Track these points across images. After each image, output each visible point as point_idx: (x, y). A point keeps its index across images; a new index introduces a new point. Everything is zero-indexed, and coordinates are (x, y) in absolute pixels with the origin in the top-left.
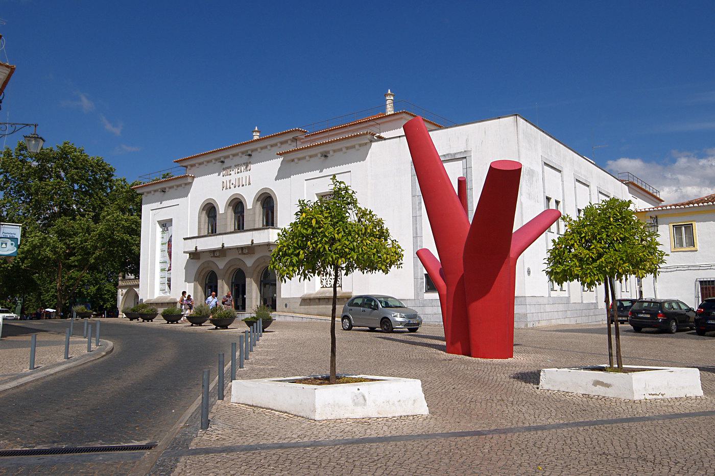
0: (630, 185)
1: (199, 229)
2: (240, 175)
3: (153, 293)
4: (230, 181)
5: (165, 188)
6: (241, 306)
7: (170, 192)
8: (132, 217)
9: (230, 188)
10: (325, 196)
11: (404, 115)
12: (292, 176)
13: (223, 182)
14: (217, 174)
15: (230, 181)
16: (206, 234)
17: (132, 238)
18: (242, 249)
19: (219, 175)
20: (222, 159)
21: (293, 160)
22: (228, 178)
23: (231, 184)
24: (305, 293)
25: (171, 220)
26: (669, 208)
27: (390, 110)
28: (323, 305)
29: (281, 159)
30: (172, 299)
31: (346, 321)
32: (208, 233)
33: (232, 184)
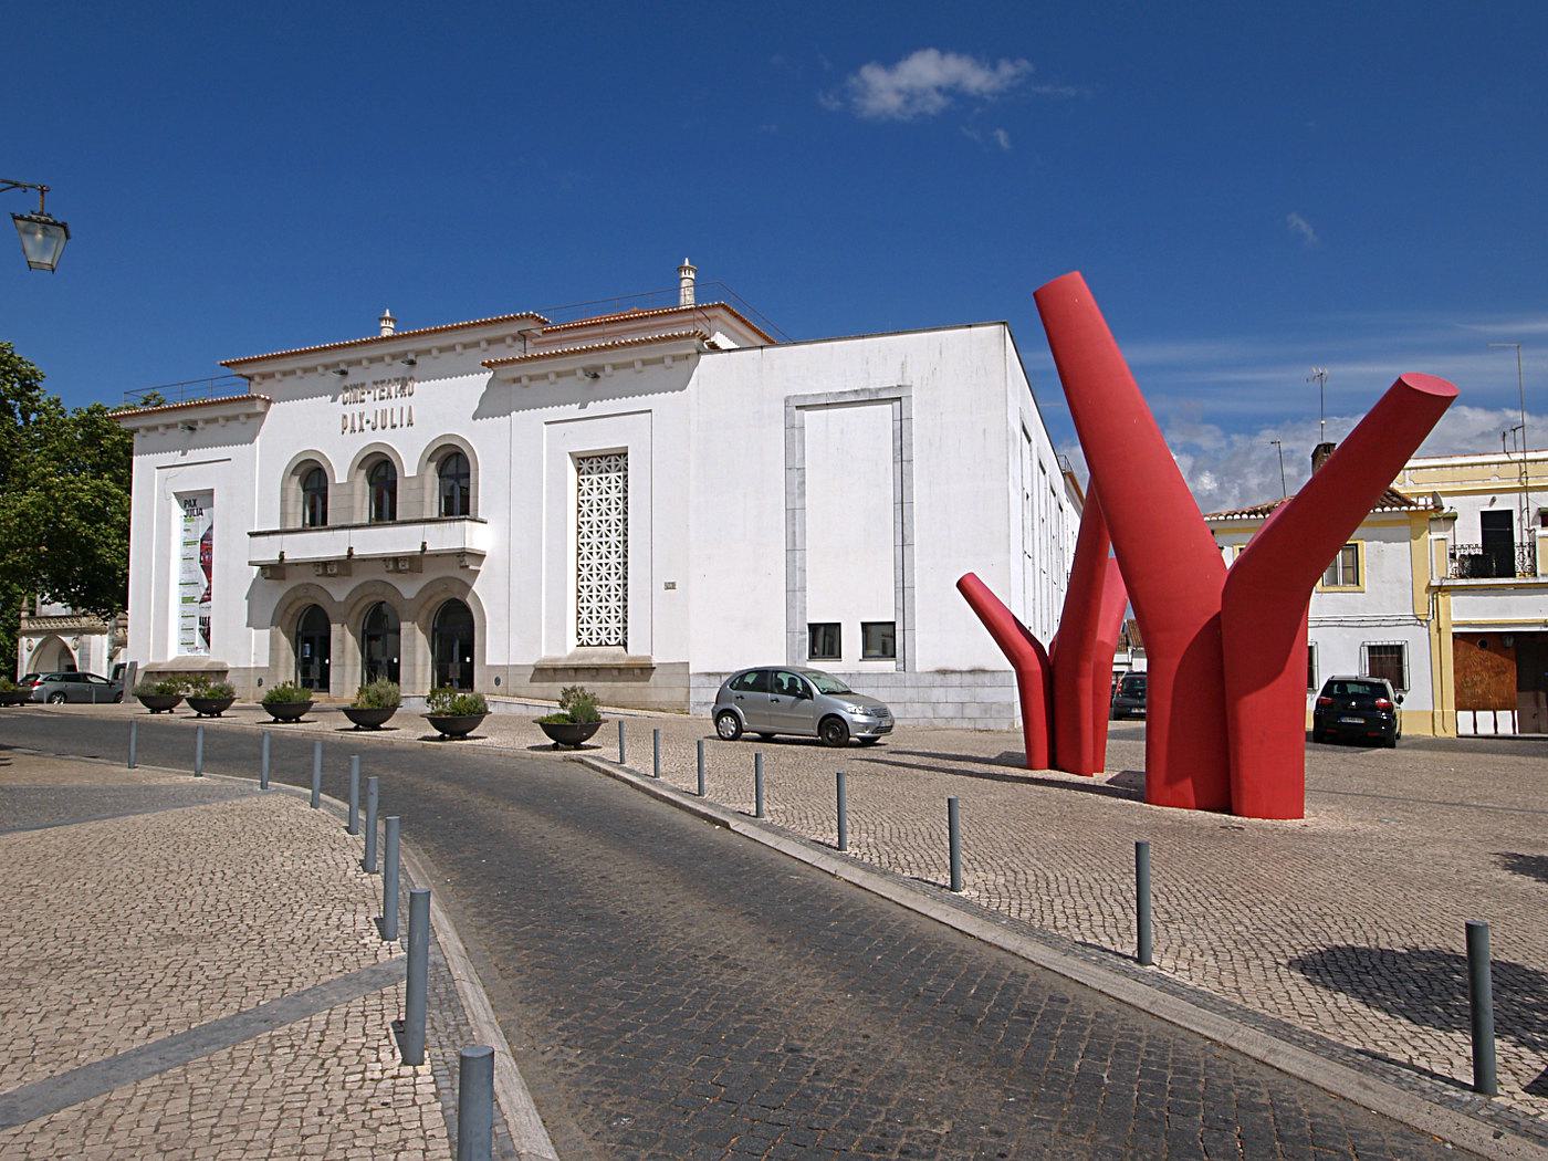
0: (1068, 480)
1: (284, 515)
2: (386, 404)
3: (164, 650)
4: (361, 416)
5: (196, 422)
6: (319, 681)
7: (204, 432)
8: (98, 482)
9: (362, 430)
10: (588, 458)
11: (721, 312)
12: (513, 413)
13: (345, 417)
14: (329, 398)
15: (361, 416)
16: (300, 526)
17: (97, 530)
18: (324, 566)
19: (334, 400)
20: (343, 367)
21: (517, 380)
22: (358, 408)
23: (364, 422)
25: (210, 493)
27: (687, 298)
28: (604, 681)
29: (489, 375)
30: (213, 663)
31: (728, 721)
33: (368, 422)
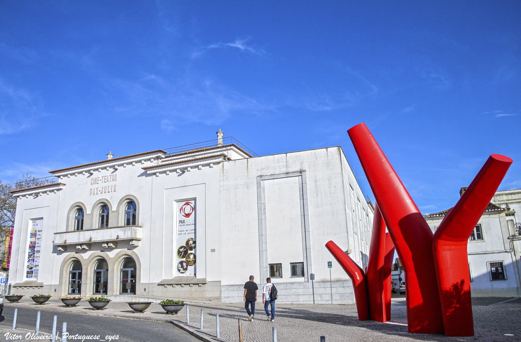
1: (67, 226)
4: (97, 189)
11: (232, 147)
15: (97, 189)
23: (98, 191)
24: (163, 279)
26: (435, 216)
27: (220, 141)
32: (74, 230)
